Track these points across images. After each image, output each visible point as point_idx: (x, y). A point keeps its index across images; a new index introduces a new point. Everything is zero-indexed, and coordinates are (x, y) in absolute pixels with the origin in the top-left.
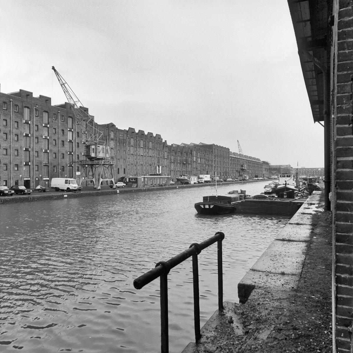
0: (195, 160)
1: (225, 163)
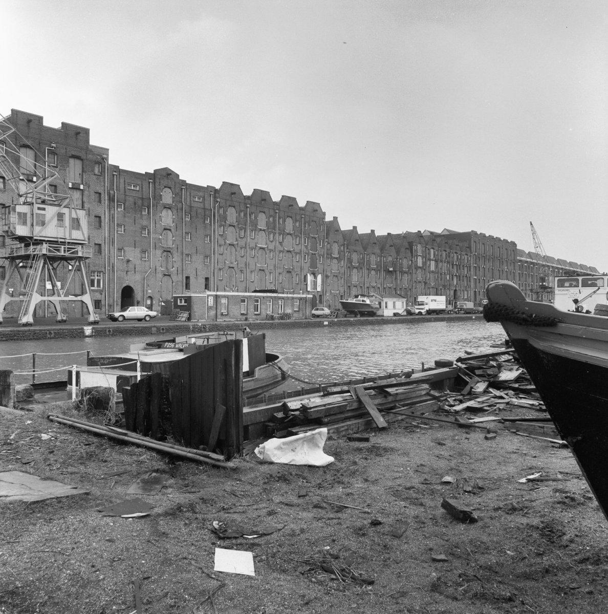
0: (420, 263)
1: (524, 276)
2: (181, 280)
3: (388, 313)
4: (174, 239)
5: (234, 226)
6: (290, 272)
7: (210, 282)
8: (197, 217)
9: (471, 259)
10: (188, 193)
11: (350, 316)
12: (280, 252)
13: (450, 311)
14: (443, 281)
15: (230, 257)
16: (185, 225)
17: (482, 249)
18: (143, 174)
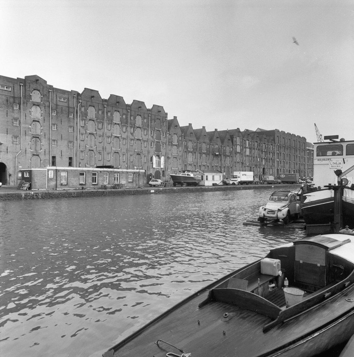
2: (48, 159)
3: (208, 183)
4: (42, 128)
5: (93, 120)
6: (140, 154)
7: (73, 160)
8: (62, 113)
9: (275, 148)
10: (55, 95)
11: (178, 185)
12: (131, 140)
13: (257, 182)
14: (255, 162)
15: (90, 142)
16: (52, 118)
17: (282, 141)
18: (15, 79)
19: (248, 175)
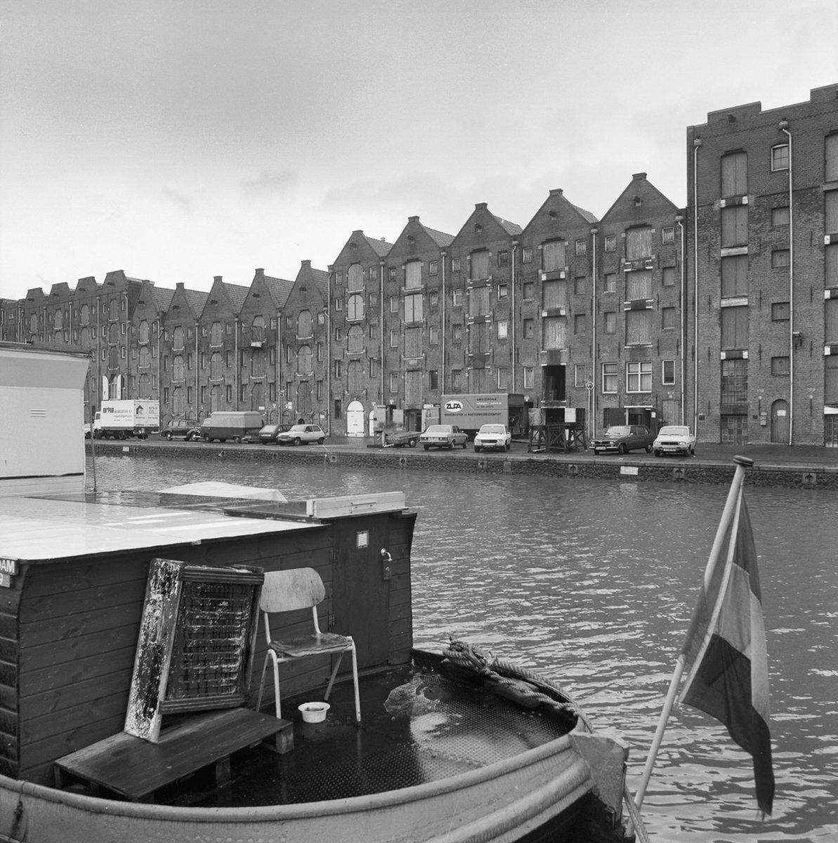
19: (119, 412)
